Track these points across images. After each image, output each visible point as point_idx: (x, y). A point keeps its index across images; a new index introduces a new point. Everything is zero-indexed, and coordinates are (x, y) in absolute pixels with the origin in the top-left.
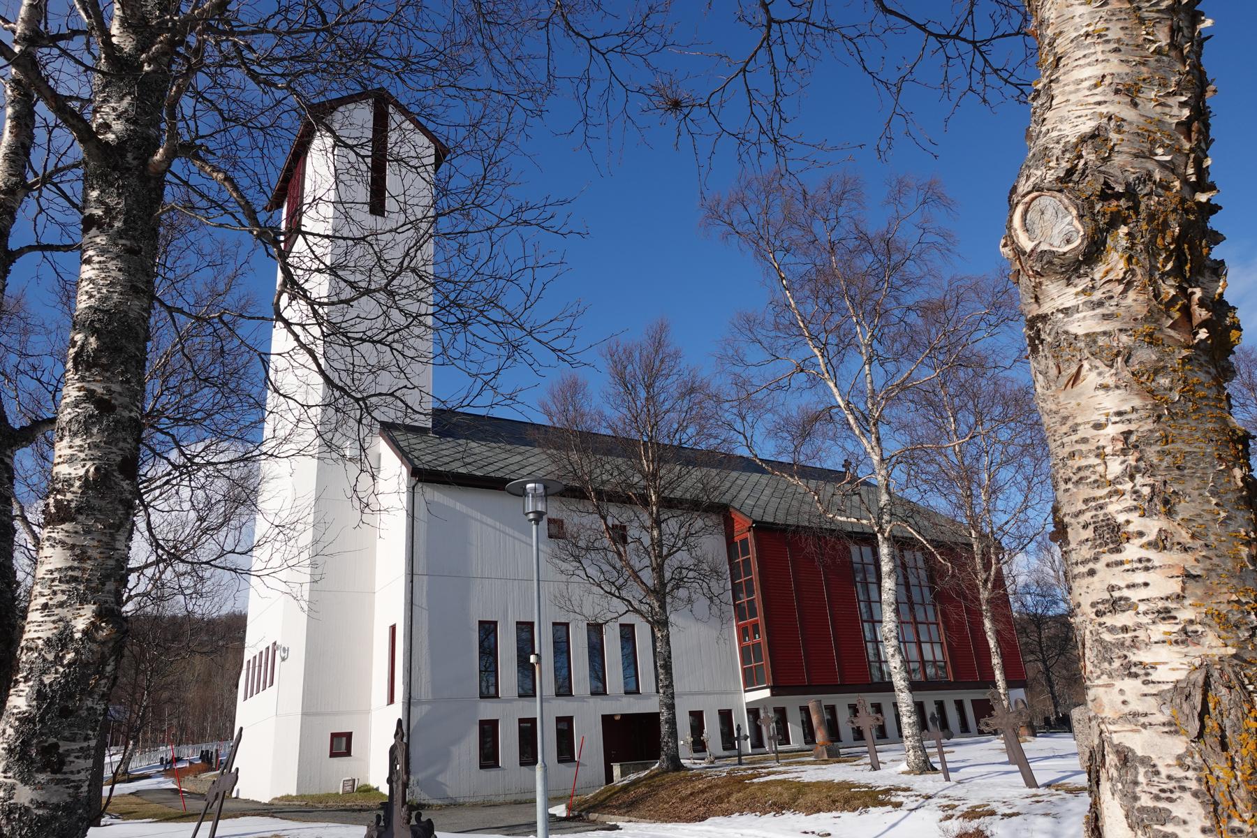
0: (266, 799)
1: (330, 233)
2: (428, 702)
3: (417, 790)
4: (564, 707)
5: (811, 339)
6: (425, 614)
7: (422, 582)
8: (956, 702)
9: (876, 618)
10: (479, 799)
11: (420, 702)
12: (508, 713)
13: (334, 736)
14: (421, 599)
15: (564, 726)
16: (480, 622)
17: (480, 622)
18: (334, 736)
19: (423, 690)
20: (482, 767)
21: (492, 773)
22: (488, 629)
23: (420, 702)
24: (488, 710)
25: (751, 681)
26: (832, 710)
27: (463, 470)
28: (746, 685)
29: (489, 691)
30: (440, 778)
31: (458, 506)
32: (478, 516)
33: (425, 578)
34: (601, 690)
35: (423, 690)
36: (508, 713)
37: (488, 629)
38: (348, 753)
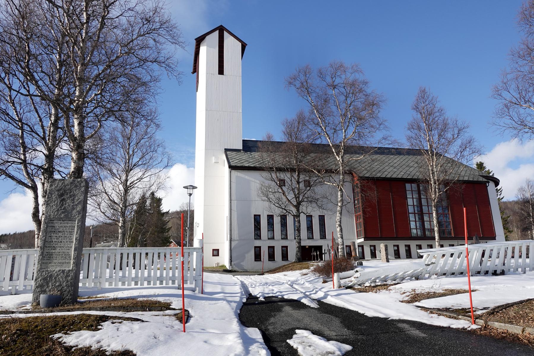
0: (207, 37)
1: (181, 299)
2: (237, 240)
3: (234, 266)
4: (285, 243)
5: (41, 347)
6: (236, 213)
7: (234, 203)
8: (406, 246)
9: (430, 212)
10: (255, 270)
11: (234, 240)
12: (264, 244)
13: (213, 250)
14: (234, 208)
15: (396, 248)
16: (254, 215)
17: (254, 215)
18: (213, 250)
19: (235, 236)
20: (255, 261)
21: (259, 263)
22: (257, 219)
23: (234, 240)
24: (258, 243)
25: (358, 237)
26: (408, 246)
27: (247, 165)
28: (357, 237)
29: (258, 236)
30: (242, 263)
31: (246, 177)
32: (253, 180)
33: (236, 201)
34: (311, 237)
35: (235, 236)
36: (264, 244)
37: (257, 219)
38: (218, 255)
